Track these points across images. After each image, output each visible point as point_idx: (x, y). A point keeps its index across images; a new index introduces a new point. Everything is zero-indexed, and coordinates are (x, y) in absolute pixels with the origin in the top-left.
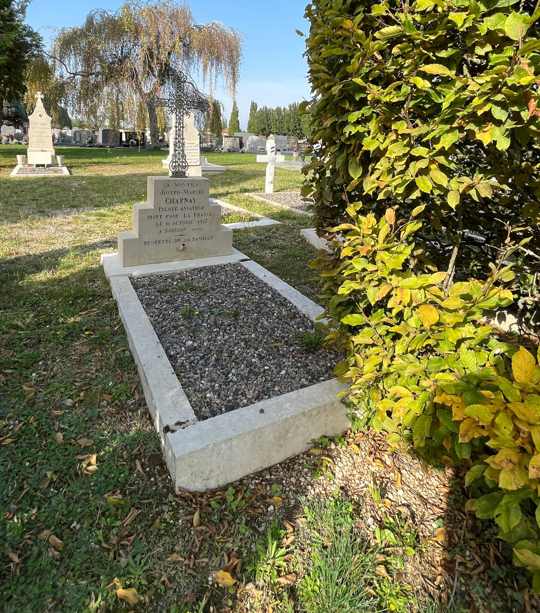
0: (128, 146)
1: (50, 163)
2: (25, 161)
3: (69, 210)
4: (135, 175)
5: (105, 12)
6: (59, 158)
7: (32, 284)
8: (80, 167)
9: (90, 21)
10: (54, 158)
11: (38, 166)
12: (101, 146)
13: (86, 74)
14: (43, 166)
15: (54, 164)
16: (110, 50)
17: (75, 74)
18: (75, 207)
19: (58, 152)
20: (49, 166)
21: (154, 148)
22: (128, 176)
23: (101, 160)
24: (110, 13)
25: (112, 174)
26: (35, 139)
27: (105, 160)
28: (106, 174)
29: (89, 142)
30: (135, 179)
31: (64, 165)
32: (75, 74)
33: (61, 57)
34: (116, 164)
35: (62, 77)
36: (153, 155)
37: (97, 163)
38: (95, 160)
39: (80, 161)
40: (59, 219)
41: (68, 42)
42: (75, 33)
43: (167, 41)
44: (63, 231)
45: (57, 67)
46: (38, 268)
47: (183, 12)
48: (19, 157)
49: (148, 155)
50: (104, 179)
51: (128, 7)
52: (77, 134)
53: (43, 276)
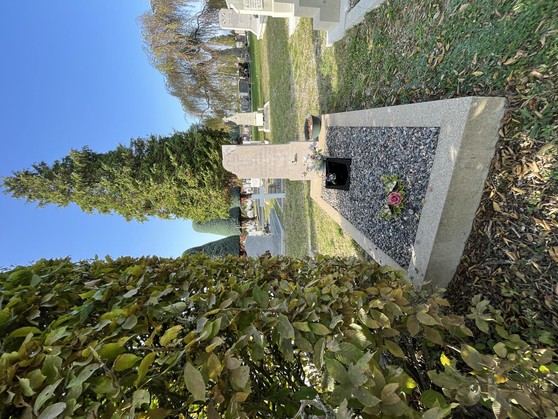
0: (248, 74)
1: (262, 114)
2: (262, 127)
3: (292, 91)
4: (269, 57)
5: (166, 85)
6: (259, 109)
7: (338, 86)
8: (264, 98)
9: (174, 94)
10: (259, 112)
11: (264, 121)
12: (250, 93)
13: (207, 96)
14: (264, 118)
15: (262, 112)
16: (188, 81)
17: (209, 104)
18: (290, 87)
19: (255, 110)
20: (264, 115)
21: (248, 51)
22: (270, 63)
23: (259, 87)
24: (166, 81)
25: (268, 76)
26: (249, 122)
27: (259, 84)
28: (268, 78)
29: (248, 100)
30: (272, 55)
31: (263, 107)
32: (209, 104)
33: (200, 112)
34: (261, 76)
35: (212, 112)
36: (254, 51)
37: (261, 89)
38: (259, 91)
39: (260, 99)
40: (297, 94)
41: (191, 107)
42: (184, 104)
43: (172, 37)
44: (304, 89)
45: (207, 115)
46: (329, 87)
47: (146, 22)
48: (259, 130)
49: (254, 55)
50: (272, 78)
51: (157, 67)
52: (244, 107)
53: (334, 83)
